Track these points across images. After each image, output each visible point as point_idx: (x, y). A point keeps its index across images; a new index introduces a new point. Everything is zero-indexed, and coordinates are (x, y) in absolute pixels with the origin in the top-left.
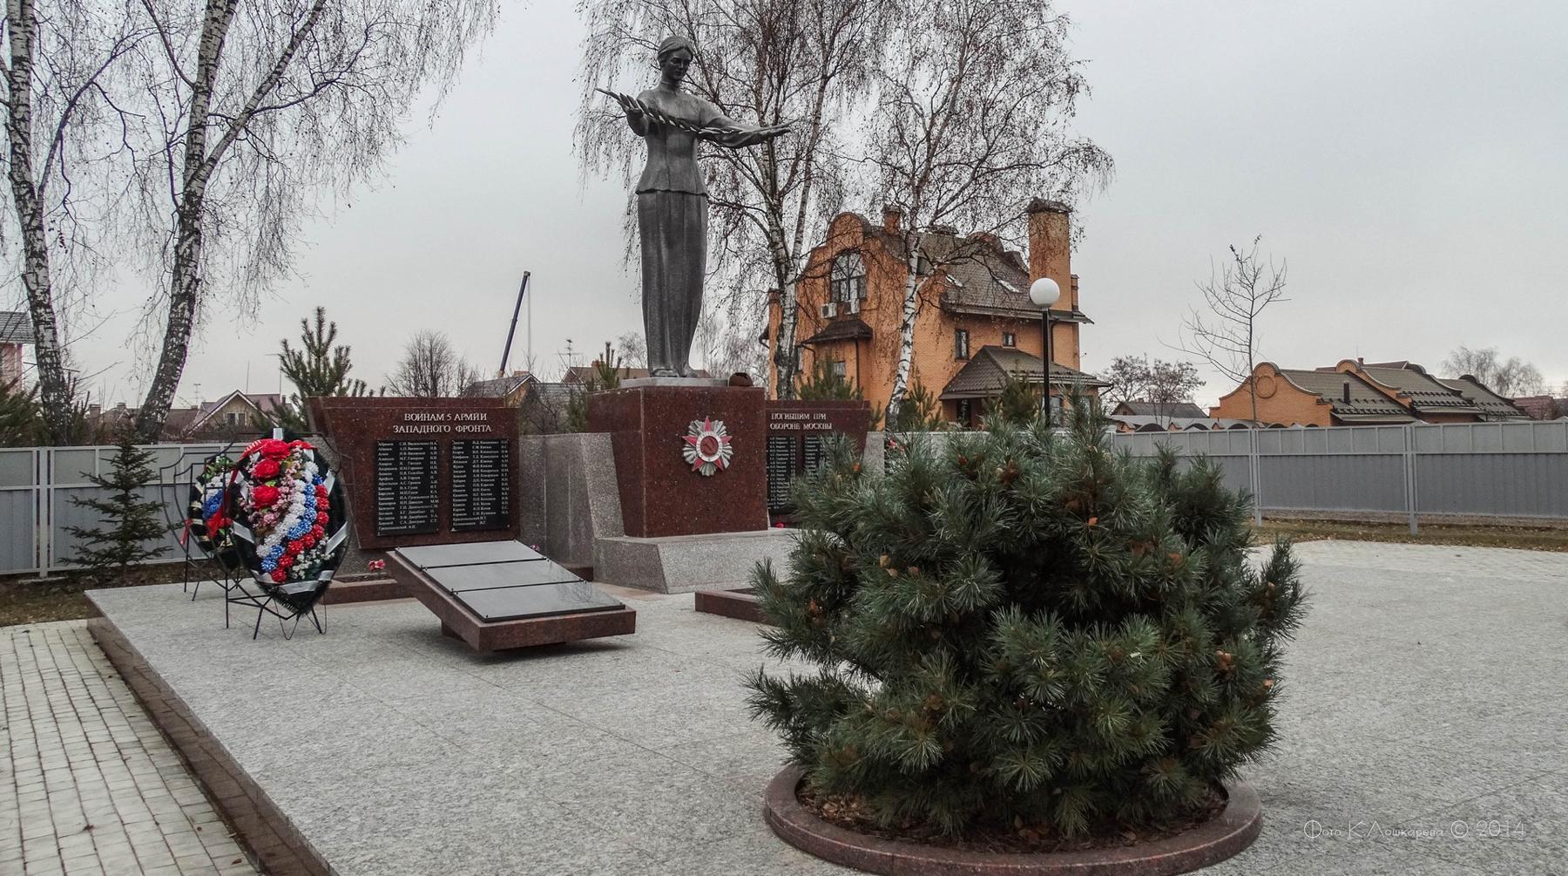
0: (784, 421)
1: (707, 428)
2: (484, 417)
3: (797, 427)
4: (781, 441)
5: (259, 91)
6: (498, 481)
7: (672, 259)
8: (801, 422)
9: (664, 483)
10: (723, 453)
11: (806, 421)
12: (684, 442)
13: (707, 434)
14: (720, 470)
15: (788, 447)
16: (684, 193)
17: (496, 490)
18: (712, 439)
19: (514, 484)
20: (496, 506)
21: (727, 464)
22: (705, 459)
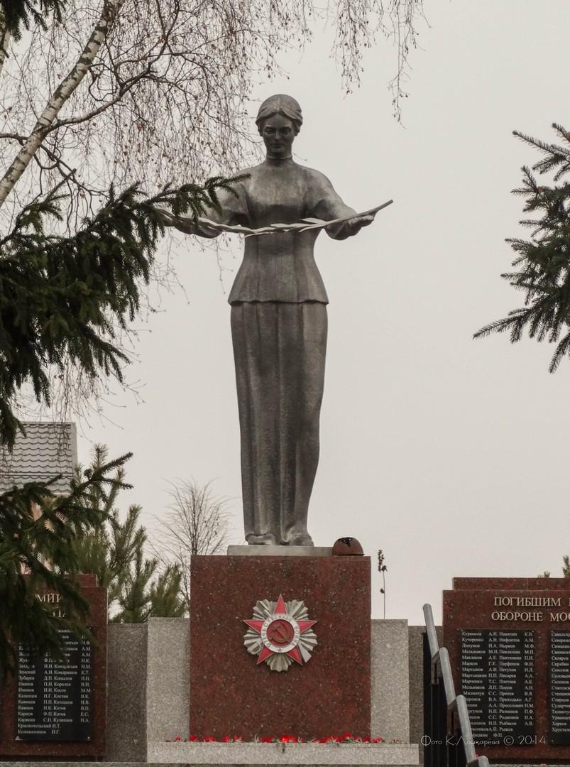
0: (515, 608)
1: (279, 610)
2: (480, 634)
3: (537, 616)
4: (508, 639)
5: (58, 94)
6: (76, 680)
7: (264, 391)
8: (546, 610)
9: (216, 678)
10: (303, 643)
11: (555, 609)
12: (246, 627)
13: (277, 617)
14: (297, 664)
15: (520, 646)
16: (277, 303)
17: (74, 691)
18: (284, 624)
19: (96, 685)
20: (73, 711)
21: (307, 656)
22: (274, 649)
